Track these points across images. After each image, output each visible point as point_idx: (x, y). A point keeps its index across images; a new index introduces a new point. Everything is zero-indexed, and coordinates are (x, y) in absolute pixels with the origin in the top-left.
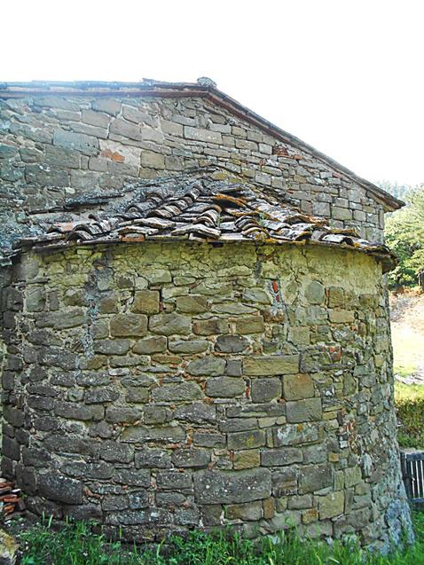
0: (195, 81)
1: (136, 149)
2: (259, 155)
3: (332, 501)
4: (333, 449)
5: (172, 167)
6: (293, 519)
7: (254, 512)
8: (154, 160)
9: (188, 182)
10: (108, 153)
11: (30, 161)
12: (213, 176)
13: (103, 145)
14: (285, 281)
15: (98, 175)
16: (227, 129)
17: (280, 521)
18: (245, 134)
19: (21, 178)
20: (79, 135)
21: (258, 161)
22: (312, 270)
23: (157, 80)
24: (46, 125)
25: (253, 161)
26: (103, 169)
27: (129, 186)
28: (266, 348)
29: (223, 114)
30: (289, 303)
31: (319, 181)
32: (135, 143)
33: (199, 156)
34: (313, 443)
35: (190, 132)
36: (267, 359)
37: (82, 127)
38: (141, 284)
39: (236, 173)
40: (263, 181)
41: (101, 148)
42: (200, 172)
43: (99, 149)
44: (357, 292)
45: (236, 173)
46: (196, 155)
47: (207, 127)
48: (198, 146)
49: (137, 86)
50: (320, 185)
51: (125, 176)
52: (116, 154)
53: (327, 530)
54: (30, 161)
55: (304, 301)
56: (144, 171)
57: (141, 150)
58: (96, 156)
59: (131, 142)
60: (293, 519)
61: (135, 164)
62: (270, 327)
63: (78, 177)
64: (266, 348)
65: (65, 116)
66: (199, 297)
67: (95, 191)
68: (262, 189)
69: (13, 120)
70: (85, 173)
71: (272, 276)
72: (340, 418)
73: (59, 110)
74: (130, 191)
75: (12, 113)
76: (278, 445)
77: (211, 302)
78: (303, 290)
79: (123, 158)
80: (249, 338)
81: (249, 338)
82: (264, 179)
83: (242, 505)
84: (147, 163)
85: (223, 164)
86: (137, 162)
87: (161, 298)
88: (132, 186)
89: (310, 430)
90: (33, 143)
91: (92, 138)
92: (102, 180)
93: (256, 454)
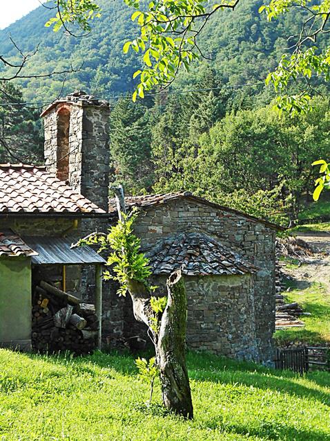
3: (218, 345)
4: (218, 331)
6: (205, 348)
7: (194, 345)
8: (166, 229)
12: (190, 231)
14: (205, 285)
16: (197, 209)
17: (201, 348)
22: (214, 281)
28: (199, 303)
31: (239, 225)
34: (211, 329)
35: (181, 214)
40: (211, 229)
44: (231, 286)
47: (188, 211)
53: (215, 352)
60: (205, 348)
62: (200, 297)
64: (199, 303)
66: (299, 228)
72: (221, 323)
74: (159, 243)
76: (201, 328)
82: (212, 228)
83: (191, 343)
86: (161, 231)
89: (211, 325)
93: (195, 331)
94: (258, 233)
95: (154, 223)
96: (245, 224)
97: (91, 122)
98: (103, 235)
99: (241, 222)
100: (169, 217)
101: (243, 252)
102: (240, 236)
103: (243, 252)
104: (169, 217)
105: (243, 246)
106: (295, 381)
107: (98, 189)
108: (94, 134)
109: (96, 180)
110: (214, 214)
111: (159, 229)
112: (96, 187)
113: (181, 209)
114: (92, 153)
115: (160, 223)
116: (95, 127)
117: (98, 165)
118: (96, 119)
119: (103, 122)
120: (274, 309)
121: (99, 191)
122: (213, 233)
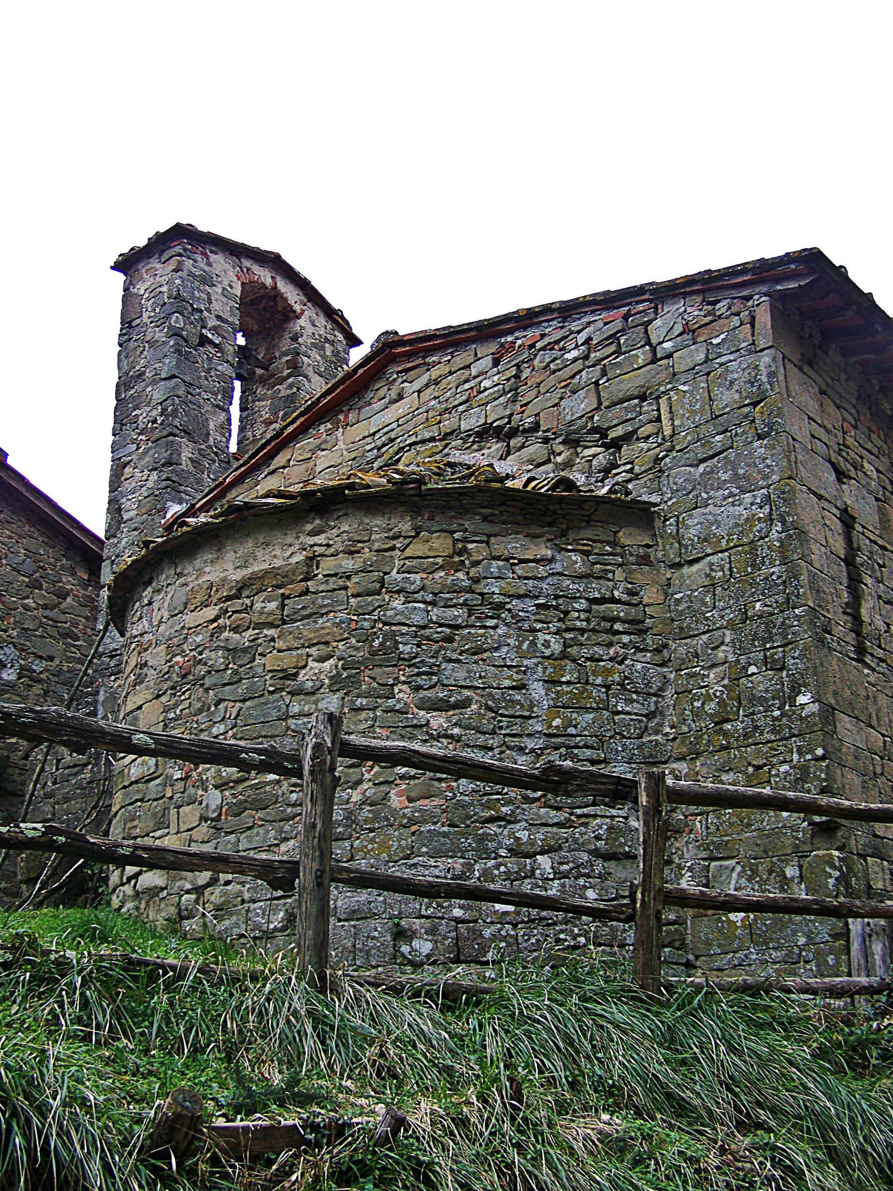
29: (420, 361)
85: (413, 439)
101: (602, 459)
120: (722, 704)
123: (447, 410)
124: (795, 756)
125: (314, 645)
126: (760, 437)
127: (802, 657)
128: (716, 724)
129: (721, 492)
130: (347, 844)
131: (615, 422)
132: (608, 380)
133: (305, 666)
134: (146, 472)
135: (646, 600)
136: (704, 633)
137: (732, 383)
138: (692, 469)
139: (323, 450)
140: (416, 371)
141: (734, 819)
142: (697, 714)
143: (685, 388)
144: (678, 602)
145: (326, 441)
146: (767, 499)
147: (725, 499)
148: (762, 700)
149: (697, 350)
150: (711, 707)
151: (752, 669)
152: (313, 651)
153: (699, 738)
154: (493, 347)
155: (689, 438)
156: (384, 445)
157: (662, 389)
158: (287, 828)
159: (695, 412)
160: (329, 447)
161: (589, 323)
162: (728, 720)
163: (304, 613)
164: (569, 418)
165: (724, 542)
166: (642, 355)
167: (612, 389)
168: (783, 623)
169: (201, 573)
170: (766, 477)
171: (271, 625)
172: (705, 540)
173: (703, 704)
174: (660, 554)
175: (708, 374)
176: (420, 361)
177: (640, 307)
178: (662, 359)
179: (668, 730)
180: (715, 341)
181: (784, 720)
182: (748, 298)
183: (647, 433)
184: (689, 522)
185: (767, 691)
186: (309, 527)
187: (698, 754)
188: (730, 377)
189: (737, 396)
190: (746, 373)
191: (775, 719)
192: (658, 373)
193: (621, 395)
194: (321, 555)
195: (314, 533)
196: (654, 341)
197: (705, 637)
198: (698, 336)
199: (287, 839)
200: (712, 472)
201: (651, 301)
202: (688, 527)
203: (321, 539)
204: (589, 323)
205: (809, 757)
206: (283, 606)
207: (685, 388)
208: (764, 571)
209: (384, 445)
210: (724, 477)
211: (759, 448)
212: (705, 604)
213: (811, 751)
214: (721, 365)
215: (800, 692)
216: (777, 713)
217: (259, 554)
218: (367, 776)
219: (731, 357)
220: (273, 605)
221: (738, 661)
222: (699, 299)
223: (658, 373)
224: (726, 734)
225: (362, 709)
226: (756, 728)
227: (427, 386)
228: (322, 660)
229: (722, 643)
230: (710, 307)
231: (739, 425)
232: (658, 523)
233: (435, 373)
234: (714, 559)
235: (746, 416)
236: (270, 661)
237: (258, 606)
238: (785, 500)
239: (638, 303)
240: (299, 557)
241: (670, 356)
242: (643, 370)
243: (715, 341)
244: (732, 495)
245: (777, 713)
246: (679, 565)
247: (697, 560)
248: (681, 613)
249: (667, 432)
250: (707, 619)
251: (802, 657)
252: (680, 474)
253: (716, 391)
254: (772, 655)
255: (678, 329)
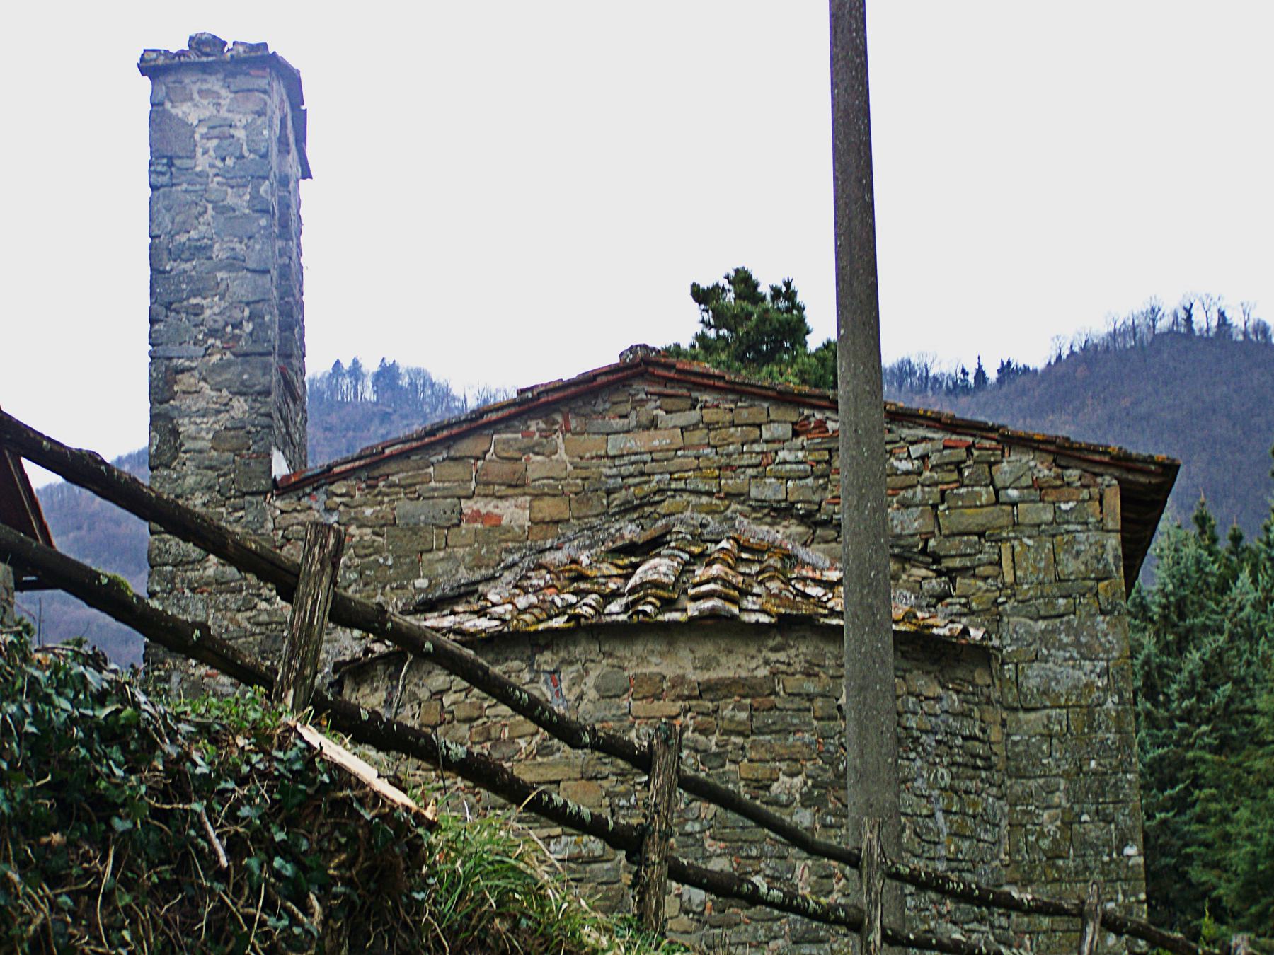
0: (616, 360)
1: (520, 500)
2: (764, 447)
5: (584, 511)
8: (549, 508)
9: (613, 531)
10: (476, 516)
11: (366, 556)
13: (468, 506)
15: (460, 552)
16: (694, 415)
18: (728, 417)
19: (355, 581)
20: (431, 502)
21: (755, 460)
23: (545, 382)
24: (386, 499)
25: (744, 463)
26: (469, 542)
27: (510, 559)
29: (684, 391)
30: (572, 697)
32: (518, 491)
33: (637, 480)
36: (540, 764)
37: (435, 489)
38: (424, 694)
39: (710, 494)
40: (768, 494)
41: (465, 511)
42: (635, 508)
43: (461, 513)
45: (710, 494)
46: (631, 481)
48: (632, 463)
49: (511, 404)
50: (907, 473)
51: (504, 545)
52: (488, 514)
54: (366, 556)
55: (592, 694)
56: (536, 529)
57: (528, 498)
58: (458, 525)
59: (510, 491)
61: (521, 522)
63: (431, 562)
65: (409, 481)
67: (459, 576)
68: (766, 511)
69: (342, 508)
70: (441, 554)
71: (547, 668)
73: (401, 475)
75: (338, 500)
77: (485, 705)
78: (590, 680)
79: (500, 517)
80: (522, 743)
81: (522, 743)
82: (769, 490)
84: (540, 516)
85: (681, 485)
86: (524, 517)
87: (443, 707)
88: (516, 557)
90: (369, 531)
91: (449, 500)
92: (467, 559)
94: (1013, 493)
95: (487, 488)
96: (934, 459)
97: (184, 123)
98: (896, 622)
99: (916, 450)
100: (562, 454)
101: (935, 584)
102: (915, 511)
103: (935, 584)
104: (562, 454)
105: (937, 559)
106: (367, 752)
107: (223, 366)
108: (202, 163)
109: (212, 333)
110: (784, 430)
111: (514, 513)
112: (216, 358)
113: (618, 423)
114: (193, 234)
115: (517, 484)
116: (207, 137)
117: (220, 275)
118: (207, 110)
119: (235, 118)
120: (1055, 841)
121: (227, 376)
122: (781, 511)
123: (729, 467)
124: (1121, 897)
125: (784, 760)
126: (1103, 612)
127: (1130, 816)
128: (1048, 859)
129: (1061, 653)
130: (827, 946)
131: (953, 552)
132: (948, 508)
133: (777, 780)
134: (225, 393)
135: (993, 739)
136: (1040, 777)
137: (1078, 553)
138: (1031, 623)
139: (537, 454)
140: (676, 401)
141: (1064, 941)
142: (1031, 848)
143: (1030, 542)
144: (1015, 744)
145: (539, 444)
146: (1106, 672)
147: (1065, 660)
148: (1093, 846)
149: (1044, 509)
150: (1045, 843)
151: (1085, 818)
152: (784, 766)
153: (1032, 870)
154: (793, 416)
155: (1031, 593)
156: (631, 476)
157: (1004, 534)
158: (775, 928)
159: (1039, 570)
160: (547, 451)
161: (924, 439)
162: (1061, 857)
163: (774, 728)
164: (898, 530)
165: (1063, 701)
166: (985, 494)
167: (951, 519)
168: (1115, 784)
169: (643, 660)
170: (1107, 651)
171: (740, 734)
172: (1044, 693)
173: (1037, 840)
174: (997, 694)
175: (1054, 536)
176: (684, 391)
177: (987, 444)
178: (1004, 503)
179: (1002, 856)
180: (1064, 507)
181: (1113, 866)
182: (1096, 475)
183: (986, 574)
184: (1029, 673)
185: (1098, 838)
186: (771, 643)
187: (1031, 882)
188: (1076, 547)
189: (1083, 568)
190: (1093, 549)
191: (1103, 863)
192: (999, 517)
193: (961, 528)
194: (783, 673)
195: (775, 649)
196: (999, 484)
197: (1041, 781)
198: (1046, 494)
199: (775, 938)
200: (1053, 631)
201: (998, 442)
202: (1026, 677)
203: (781, 656)
204: (924, 439)
205: (1133, 899)
206: (751, 717)
207: (1030, 542)
208: (1100, 734)
209: (631, 476)
210: (1065, 639)
211: (1101, 622)
212: (1043, 752)
213: (1136, 895)
214: (1068, 532)
215: (1126, 845)
216: (1106, 859)
217: (723, 660)
218: (836, 887)
219: (1079, 528)
220: (743, 715)
221: (1072, 808)
222: (1051, 458)
223: (999, 517)
224: (1058, 869)
225: (831, 826)
226: (1087, 868)
227: (696, 426)
228: (792, 775)
229: (1058, 789)
230: (1060, 471)
231: (1084, 595)
232: (995, 665)
233: (710, 415)
234: (1053, 712)
235: (1091, 589)
236: (744, 769)
237: (727, 713)
238: (1123, 677)
239: (987, 438)
240: (763, 672)
241: (1014, 504)
242: (985, 510)
243: (1064, 507)
244: (1072, 658)
245: (1106, 859)
246: (1015, 710)
247: (1034, 709)
248: (1018, 754)
249: (1009, 579)
250: (1043, 765)
251: (1130, 816)
252: (1017, 623)
253: (1062, 556)
254: (1104, 810)
255: (1026, 481)
